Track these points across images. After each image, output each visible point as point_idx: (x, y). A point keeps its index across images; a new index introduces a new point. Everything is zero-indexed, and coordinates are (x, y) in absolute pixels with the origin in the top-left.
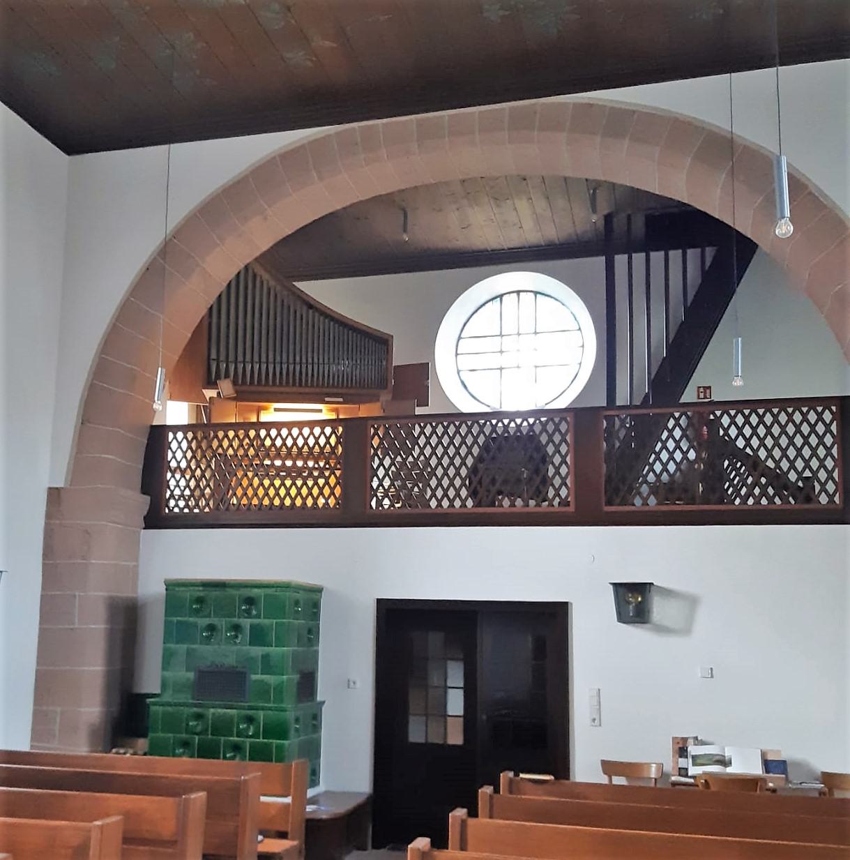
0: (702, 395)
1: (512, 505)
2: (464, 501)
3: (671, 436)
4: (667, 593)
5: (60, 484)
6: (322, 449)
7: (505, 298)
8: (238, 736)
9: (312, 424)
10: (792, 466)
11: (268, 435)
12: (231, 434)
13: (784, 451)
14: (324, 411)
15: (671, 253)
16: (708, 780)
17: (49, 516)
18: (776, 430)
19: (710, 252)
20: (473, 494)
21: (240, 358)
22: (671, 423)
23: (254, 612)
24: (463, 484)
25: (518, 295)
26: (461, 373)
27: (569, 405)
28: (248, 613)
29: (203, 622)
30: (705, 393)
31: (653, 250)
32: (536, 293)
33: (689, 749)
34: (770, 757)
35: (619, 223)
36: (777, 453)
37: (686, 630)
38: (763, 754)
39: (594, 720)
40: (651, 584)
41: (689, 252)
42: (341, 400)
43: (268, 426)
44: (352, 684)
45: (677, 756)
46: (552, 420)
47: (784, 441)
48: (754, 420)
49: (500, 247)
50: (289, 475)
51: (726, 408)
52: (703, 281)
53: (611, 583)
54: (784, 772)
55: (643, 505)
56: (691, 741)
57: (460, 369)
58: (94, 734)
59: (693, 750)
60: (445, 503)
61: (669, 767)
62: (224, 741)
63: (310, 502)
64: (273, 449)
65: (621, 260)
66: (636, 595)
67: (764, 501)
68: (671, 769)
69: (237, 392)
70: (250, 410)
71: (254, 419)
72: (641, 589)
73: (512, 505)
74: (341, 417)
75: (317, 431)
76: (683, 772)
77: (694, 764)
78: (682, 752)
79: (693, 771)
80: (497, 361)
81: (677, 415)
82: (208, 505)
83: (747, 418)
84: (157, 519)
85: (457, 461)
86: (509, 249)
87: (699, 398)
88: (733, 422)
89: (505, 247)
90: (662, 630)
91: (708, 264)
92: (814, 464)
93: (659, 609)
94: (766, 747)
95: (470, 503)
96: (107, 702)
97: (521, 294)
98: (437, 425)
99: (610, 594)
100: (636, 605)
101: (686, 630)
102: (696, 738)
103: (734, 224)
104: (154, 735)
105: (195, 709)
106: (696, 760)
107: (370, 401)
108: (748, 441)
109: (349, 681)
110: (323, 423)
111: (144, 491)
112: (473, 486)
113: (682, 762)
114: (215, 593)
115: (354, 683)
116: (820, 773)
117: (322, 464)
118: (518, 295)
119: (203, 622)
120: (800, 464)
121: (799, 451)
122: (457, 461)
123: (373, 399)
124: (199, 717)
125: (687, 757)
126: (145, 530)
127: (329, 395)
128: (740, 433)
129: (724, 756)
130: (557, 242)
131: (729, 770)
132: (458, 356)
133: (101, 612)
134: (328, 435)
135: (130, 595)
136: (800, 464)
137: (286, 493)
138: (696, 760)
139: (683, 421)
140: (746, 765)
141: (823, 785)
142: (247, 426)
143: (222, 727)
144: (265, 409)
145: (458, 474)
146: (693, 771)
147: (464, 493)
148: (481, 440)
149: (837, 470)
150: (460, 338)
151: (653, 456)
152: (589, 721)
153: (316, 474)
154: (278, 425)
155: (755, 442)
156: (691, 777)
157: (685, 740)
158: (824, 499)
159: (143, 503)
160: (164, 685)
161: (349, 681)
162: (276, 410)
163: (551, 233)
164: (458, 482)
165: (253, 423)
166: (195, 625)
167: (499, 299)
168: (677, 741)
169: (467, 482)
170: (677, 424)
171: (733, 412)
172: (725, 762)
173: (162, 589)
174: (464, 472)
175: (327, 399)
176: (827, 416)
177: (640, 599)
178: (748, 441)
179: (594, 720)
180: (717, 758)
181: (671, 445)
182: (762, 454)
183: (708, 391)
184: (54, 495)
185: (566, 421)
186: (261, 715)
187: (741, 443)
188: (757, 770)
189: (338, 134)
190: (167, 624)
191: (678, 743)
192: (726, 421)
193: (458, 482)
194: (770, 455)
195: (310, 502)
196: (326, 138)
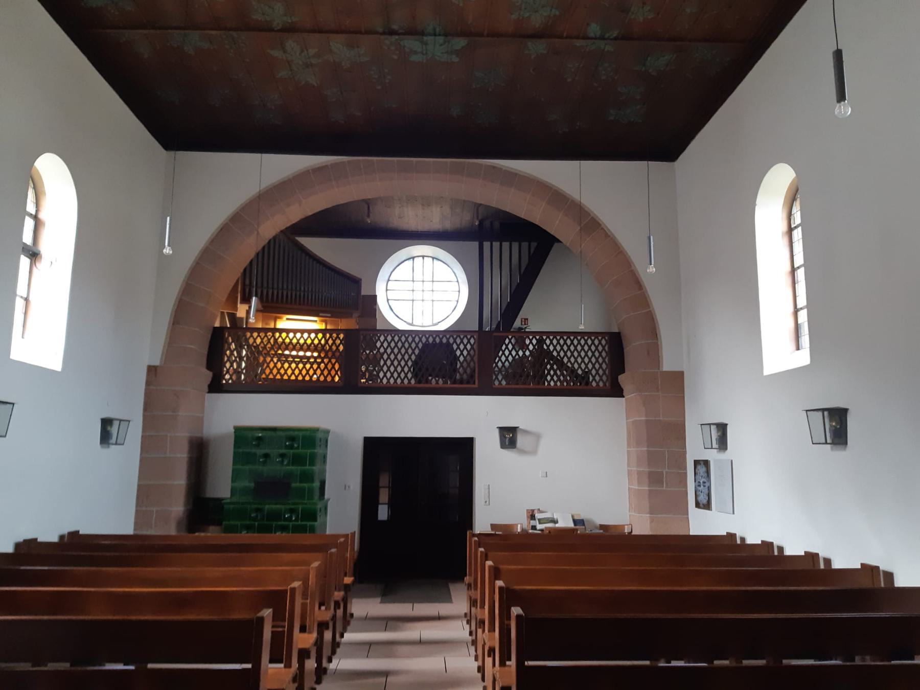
0: (523, 323)
1: (437, 383)
2: (409, 381)
3: (507, 348)
4: (525, 432)
5: (156, 362)
6: (330, 347)
7: (415, 259)
8: (284, 521)
9: (309, 332)
10: (580, 367)
11: (252, 336)
12: (262, 335)
13: (576, 359)
14: (318, 322)
15: (494, 243)
16: (550, 530)
17: (148, 383)
18: (579, 348)
19: (534, 245)
20: (415, 375)
21: (265, 285)
22: (507, 341)
23: (296, 445)
24: (409, 370)
25: (423, 258)
26: (389, 301)
27: (448, 328)
28: (291, 447)
29: (260, 452)
30: (525, 322)
31: (494, 241)
32: (433, 258)
33: (536, 515)
34: (576, 518)
35: (487, 223)
36: (572, 360)
37: (534, 452)
38: (573, 516)
39: (486, 502)
40: (518, 427)
41: (494, 243)
42: (329, 315)
43: (281, 331)
44: (347, 488)
45: (529, 519)
46: (446, 336)
47: (583, 354)
48: (589, 342)
49: (416, 230)
50: (301, 361)
51: (534, 335)
52: (48, 152)
53: (497, 428)
54: (584, 525)
55: (499, 384)
56: (536, 511)
57: (389, 298)
58: (179, 524)
59: (538, 516)
60: (399, 381)
61: (525, 526)
62: (276, 525)
63: (329, 379)
64: (313, 345)
65: (487, 245)
66: (509, 434)
67: (559, 384)
68: (526, 527)
69: (263, 307)
70: (269, 318)
71: (272, 326)
72: (513, 430)
73: (437, 383)
74: (328, 328)
75: (320, 336)
76: (534, 528)
77: (540, 523)
78: (532, 517)
79: (539, 527)
80: (409, 296)
81: (510, 337)
82: (231, 378)
83: (579, 341)
84: (216, 386)
85: (406, 357)
86: (421, 232)
87: (522, 324)
88: (551, 343)
89: (419, 231)
90: (523, 452)
91: (532, 252)
92: (590, 366)
93: (521, 440)
94: (573, 513)
95: (413, 381)
96: (187, 502)
97: (425, 258)
98: (388, 335)
99: (497, 432)
100: (509, 439)
101: (534, 452)
102: (539, 509)
103: (800, 252)
104: (227, 523)
105: (255, 506)
106: (541, 521)
107: (346, 317)
108: (558, 353)
109: (345, 486)
110: (317, 332)
111: (209, 367)
112: (415, 372)
113: (533, 523)
114: (269, 433)
115: (349, 487)
116: (598, 525)
117: (322, 355)
118: (423, 258)
119: (260, 452)
120: (583, 366)
121: (590, 359)
122: (406, 357)
123: (348, 315)
124: (258, 510)
125: (535, 519)
126: (210, 395)
127: (323, 312)
128: (555, 349)
129: (554, 519)
130: (441, 230)
131: (557, 525)
132: (388, 291)
133: (185, 447)
134: (320, 338)
135: (199, 435)
136: (583, 366)
137: (291, 371)
138: (541, 521)
139: (513, 341)
140: (565, 523)
141: (602, 531)
142: (266, 330)
143: (277, 516)
144: (280, 318)
145: (406, 364)
146: (539, 527)
147: (410, 375)
148: (420, 345)
149: (607, 370)
150: (389, 280)
151: (498, 359)
152: (483, 503)
153: (319, 360)
154: (288, 331)
155: (562, 354)
156: (539, 530)
157: (533, 511)
158: (594, 384)
159: (207, 376)
160: (233, 491)
161: (345, 486)
162: (288, 319)
163: (448, 225)
164: (406, 369)
165: (260, 328)
166: (255, 454)
167: (412, 259)
168: (528, 511)
169: (412, 369)
170: (510, 342)
171: (565, 338)
172: (556, 522)
173: (233, 430)
174: (410, 363)
175: (321, 314)
176: (603, 342)
177: (511, 435)
178: (558, 353)
179: (486, 502)
180: (550, 519)
181: (507, 353)
182: (576, 366)
183: (526, 321)
184: (152, 370)
185: (474, 338)
186: (300, 507)
187: (555, 354)
188: (571, 525)
189: (349, 162)
190: (236, 455)
191: (529, 513)
192: (548, 342)
193: (406, 369)
194: (569, 361)
195: (329, 379)
196: (343, 162)
